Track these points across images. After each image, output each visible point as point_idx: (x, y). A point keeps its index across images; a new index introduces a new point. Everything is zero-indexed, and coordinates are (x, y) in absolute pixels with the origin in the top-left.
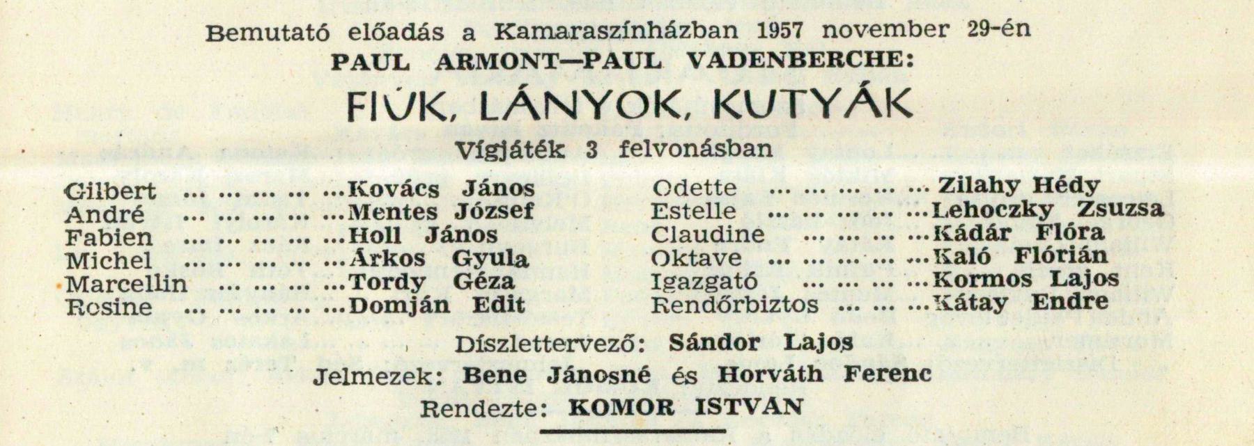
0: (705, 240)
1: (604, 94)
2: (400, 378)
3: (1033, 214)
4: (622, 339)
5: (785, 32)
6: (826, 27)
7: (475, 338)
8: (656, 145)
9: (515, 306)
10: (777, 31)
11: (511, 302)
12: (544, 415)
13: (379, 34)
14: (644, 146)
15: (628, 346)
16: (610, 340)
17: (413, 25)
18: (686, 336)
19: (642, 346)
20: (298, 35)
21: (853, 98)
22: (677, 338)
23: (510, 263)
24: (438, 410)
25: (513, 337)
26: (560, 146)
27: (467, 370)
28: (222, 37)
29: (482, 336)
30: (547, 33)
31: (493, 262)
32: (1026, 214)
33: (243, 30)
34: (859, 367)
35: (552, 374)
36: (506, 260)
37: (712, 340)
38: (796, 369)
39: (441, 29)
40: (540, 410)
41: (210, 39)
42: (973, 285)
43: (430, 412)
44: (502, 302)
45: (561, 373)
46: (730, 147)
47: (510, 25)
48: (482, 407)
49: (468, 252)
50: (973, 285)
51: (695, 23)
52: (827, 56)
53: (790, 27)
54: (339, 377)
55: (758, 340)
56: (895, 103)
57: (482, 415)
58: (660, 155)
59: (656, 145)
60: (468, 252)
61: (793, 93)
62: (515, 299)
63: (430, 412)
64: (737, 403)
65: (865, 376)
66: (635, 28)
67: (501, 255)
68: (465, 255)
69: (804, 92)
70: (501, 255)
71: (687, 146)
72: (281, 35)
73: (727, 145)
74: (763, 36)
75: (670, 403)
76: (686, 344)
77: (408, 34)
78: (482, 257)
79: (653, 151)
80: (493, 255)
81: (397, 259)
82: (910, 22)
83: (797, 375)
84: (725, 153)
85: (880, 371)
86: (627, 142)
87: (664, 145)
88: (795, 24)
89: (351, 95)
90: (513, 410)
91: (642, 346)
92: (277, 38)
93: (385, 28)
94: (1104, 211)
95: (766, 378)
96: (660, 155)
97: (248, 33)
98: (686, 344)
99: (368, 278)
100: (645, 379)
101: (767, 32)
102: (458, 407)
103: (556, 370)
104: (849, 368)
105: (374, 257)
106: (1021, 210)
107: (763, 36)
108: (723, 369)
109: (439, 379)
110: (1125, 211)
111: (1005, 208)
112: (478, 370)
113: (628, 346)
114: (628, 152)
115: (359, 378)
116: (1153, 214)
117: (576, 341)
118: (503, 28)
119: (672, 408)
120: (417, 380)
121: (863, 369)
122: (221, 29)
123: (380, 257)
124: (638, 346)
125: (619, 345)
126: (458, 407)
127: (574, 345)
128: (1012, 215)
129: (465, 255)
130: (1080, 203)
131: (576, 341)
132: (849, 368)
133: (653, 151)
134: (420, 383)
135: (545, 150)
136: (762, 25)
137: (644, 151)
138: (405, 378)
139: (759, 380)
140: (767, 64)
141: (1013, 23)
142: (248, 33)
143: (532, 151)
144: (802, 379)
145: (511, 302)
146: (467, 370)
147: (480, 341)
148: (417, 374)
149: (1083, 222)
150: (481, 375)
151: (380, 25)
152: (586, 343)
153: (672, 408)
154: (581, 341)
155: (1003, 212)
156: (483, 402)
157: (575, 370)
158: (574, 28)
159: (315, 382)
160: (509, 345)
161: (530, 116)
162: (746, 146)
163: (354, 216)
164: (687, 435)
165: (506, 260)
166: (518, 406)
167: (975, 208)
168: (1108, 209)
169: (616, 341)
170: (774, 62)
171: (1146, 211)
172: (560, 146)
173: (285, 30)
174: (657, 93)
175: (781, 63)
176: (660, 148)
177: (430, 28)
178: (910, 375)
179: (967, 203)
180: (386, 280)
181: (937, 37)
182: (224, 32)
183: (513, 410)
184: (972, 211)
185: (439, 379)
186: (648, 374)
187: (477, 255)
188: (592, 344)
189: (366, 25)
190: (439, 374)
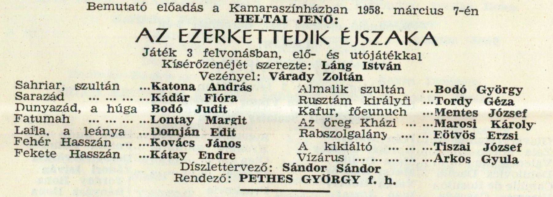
0: (390, 114)
1: (415, 41)
5: (371, 11)
6: (395, 9)
7: (190, 164)
8: (221, 52)
9: (222, 110)
10: (367, 10)
13: (171, 8)
14: (215, 51)
16: (256, 166)
17: (188, 4)
18: (291, 164)
20: (131, 8)
21: (341, 37)
22: (286, 165)
23: (509, 162)
26: (174, 51)
28: (95, 9)
30: (401, 11)
31: (501, 162)
33: (105, 5)
36: (507, 161)
39: (202, 6)
41: (89, 9)
46: (257, 53)
47: (237, 5)
49: (489, 156)
51: (327, 6)
52: (255, 17)
56: (321, 38)
58: (223, 56)
59: (221, 52)
60: (489, 156)
61: (275, 32)
66: (297, 8)
67: (505, 158)
68: (487, 158)
69: (266, 31)
70: (505, 158)
71: (236, 52)
72: (123, 7)
73: (256, 52)
76: (291, 168)
77: (186, 8)
78: (496, 159)
79: (219, 54)
80: (501, 158)
81: (457, 159)
82: (305, 5)
84: (254, 55)
86: (207, 49)
87: (225, 51)
92: (121, 9)
93: (175, 5)
96: (223, 56)
97: (107, 6)
98: (291, 168)
101: (363, 11)
105: (446, 158)
107: (360, 13)
114: (207, 54)
117: (239, 166)
118: (233, 6)
120: (30, 154)
122: (94, 4)
123: (449, 157)
129: (487, 158)
130: (324, 74)
131: (239, 166)
133: (219, 54)
134: (32, 156)
135: (167, 53)
136: (360, 7)
140: (313, 21)
141: (470, 8)
142: (107, 6)
143: (161, 53)
147: (192, 165)
148: (30, 152)
151: (172, 4)
152: (244, 167)
154: (242, 166)
158: (268, 7)
162: (265, 52)
163: (437, 125)
165: (507, 161)
170: (317, 21)
172: (174, 51)
173: (125, 5)
174: (230, 31)
175: (320, 21)
176: (223, 53)
177: (197, 5)
182: (96, 6)
187: (494, 158)
188: (247, 167)
189: (166, 4)
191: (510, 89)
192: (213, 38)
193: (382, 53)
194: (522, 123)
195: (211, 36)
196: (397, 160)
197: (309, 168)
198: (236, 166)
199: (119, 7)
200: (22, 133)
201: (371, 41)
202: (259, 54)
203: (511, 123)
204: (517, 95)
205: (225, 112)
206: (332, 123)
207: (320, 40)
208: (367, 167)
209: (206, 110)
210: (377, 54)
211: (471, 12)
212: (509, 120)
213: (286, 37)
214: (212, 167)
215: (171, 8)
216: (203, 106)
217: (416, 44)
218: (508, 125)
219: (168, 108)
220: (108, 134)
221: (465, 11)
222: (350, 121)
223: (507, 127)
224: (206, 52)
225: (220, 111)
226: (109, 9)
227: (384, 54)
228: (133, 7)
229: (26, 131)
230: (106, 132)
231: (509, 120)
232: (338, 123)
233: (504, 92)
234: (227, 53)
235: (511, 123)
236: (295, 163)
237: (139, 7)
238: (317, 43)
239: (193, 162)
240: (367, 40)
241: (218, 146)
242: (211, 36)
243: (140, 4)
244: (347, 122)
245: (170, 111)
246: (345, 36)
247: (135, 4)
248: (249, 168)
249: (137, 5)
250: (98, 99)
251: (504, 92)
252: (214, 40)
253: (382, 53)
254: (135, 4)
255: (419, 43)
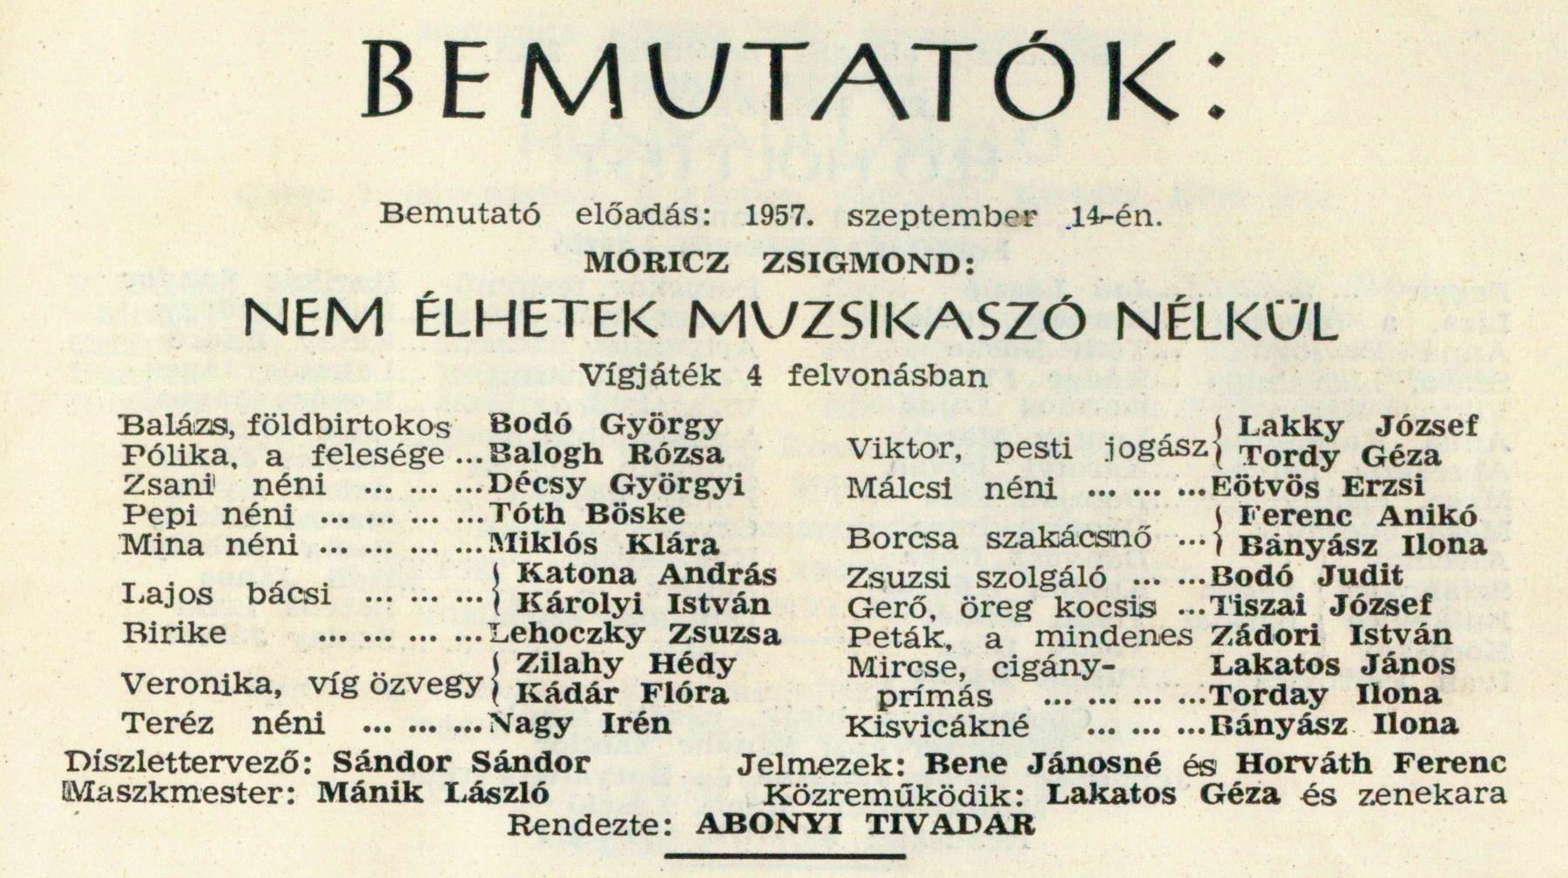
2: (850, 766)
3: (619, 640)
4: (281, 757)
5: (782, 217)
7: (92, 754)
8: (835, 370)
9: (1391, 577)
10: (771, 215)
11: (1385, 573)
12: (668, 833)
13: (614, 216)
15: (289, 765)
19: (307, 765)
21: (415, 314)
22: (341, 756)
24: (530, 826)
25: (141, 753)
27: (931, 757)
29: (99, 751)
32: (609, 640)
34: (1412, 755)
35: (1033, 761)
37: (388, 759)
38: (1337, 757)
40: (663, 827)
42: (1299, 642)
43: (520, 829)
44: (1373, 573)
45: (1046, 760)
46: (932, 373)
48: (588, 823)
50: (1299, 642)
53: (788, 210)
54: (771, 764)
55: (449, 758)
57: (588, 833)
58: (840, 382)
59: (835, 370)
62: (1391, 568)
63: (520, 829)
64: (883, 820)
65: (1421, 765)
73: (928, 370)
74: (752, 223)
75: (1029, 818)
76: (354, 763)
77: (652, 216)
79: (831, 378)
83: (1338, 765)
85: (1440, 761)
86: (800, 366)
88: (794, 207)
89: (452, 49)
90: (628, 826)
91: (307, 765)
93: (623, 209)
94: (703, 636)
95: (1298, 766)
96: (840, 382)
99: (1264, 451)
100: (1154, 769)
102: (557, 822)
103: (1039, 757)
104: (1400, 756)
106: (603, 634)
107: (752, 223)
108: (1243, 757)
109: (900, 768)
110: (730, 636)
111: (582, 631)
112: (945, 757)
113: (289, 765)
114: (800, 378)
115: (796, 766)
116: (766, 642)
117: (222, 758)
119: (1032, 825)
120: (871, 769)
121: (1418, 758)
124: (303, 765)
125: (278, 764)
126: (557, 822)
127: (219, 764)
128: (591, 641)
131: (222, 758)
132: (1400, 756)
133: (831, 378)
136: (751, 208)
137: (821, 379)
138: (856, 766)
139: (1289, 770)
142: (434, 214)
144: (1345, 771)
145: (1385, 573)
146: (931, 757)
147: (97, 758)
148: (871, 761)
149: (678, 650)
150: (949, 763)
151: (616, 204)
152: (235, 761)
153: (1032, 825)
154: (229, 758)
155: (579, 636)
156: (588, 816)
157: (1063, 757)
159: (740, 771)
160: (135, 763)
161: (1106, 106)
164: (745, 861)
166: (634, 821)
167: (544, 631)
168: (708, 633)
169: (275, 759)
171: (758, 637)
176: (841, 374)
178: (1479, 765)
179: (533, 624)
180: (1288, 453)
181: (1132, 227)
182: (404, 212)
183: (628, 826)
184: (539, 635)
185: (900, 768)
186: (1158, 763)
188: (243, 762)
190: (901, 762)
191: (698, 482)
192: (618, 325)
193: (667, 368)
194: (600, 600)
195: (313, 316)
196: (1136, 731)
197: (405, 764)
198: (214, 759)
199: (466, 216)
200: (1230, 673)
201: (1005, 328)
202: (938, 378)
203: (570, 601)
204: (716, 496)
205: (1397, 582)
206: (981, 607)
207: (894, 326)
208: (554, 759)
209: (1348, 577)
210: (654, 372)
211: (1133, 220)
212: (567, 590)
213: (598, 318)
214: (151, 763)
215: (614, 216)
216: (1339, 566)
217: (914, 335)
218: (565, 605)
219: (1254, 573)
220: (1075, 673)
221: (1118, 217)
222: (1028, 604)
223: (559, 610)
224: (794, 372)
225: (1385, 582)
226: (967, 224)
227: (673, 371)
228: (503, 215)
229: (1243, 668)
230: (1070, 667)
231: (567, 590)
232: (999, 608)
233: (682, 490)
234: (850, 374)
235: (570, 601)
236: (1059, 753)
237: (519, 216)
238: (889, 333)
239: (99, 751)
240: (996, 325)
241: (598, 700)
242: (313, 316)
243: (523, 206)
244: (1023, 607)
245: (1259, 583)
246: (426, 312)
247: (507, 208)
248: (248, 764)
249: (514, 210)
250: (344, 550)
251: (682, 490)
252: (621, 330)
253: (667, 368)
254: (507, 208)
255: (922, 331)
